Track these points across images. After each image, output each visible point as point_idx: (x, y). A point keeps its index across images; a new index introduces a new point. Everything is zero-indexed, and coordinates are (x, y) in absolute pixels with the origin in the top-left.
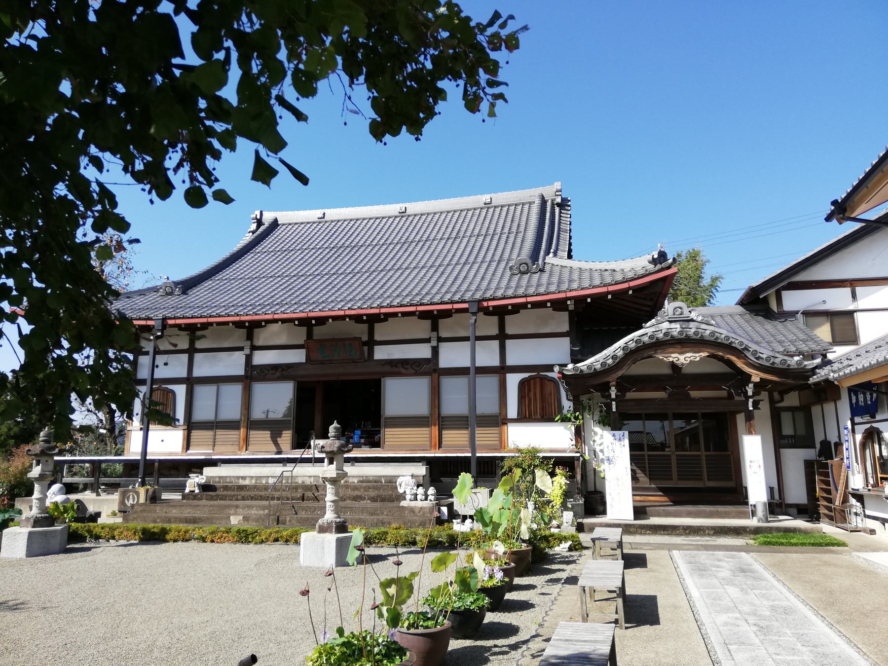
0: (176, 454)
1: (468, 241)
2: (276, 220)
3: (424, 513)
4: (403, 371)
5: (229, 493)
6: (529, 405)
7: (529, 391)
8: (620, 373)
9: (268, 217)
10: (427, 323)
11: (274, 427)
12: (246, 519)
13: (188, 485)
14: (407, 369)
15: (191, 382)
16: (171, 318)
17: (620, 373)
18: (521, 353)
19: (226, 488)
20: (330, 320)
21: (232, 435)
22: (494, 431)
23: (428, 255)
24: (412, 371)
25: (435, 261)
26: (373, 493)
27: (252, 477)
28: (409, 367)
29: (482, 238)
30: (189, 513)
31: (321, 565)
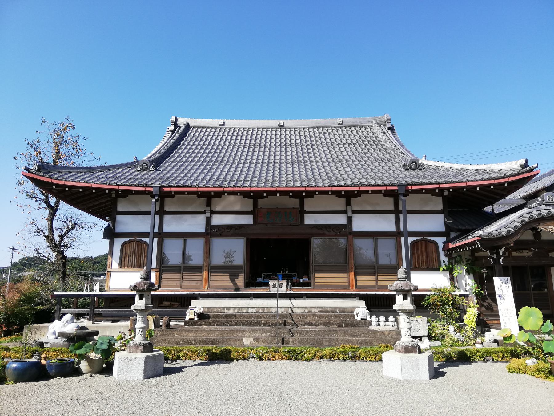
1: (190, 148)
2: (188, 124)
3: (392, 335)
4: (327, 233)
5: (220, 320)
6: (418, 257)
7: (418, 249)
8: (516, 238)
9: (182, 122)
10: (204, 200)
11: (231, 270)
12: (256, 340)
13: (188, 314)
14: (330, 231)
16: (166, 187)
17: (516, 238)
18: (417, 224)
19: (218, 316)
20: (278, 195)
21: (196, 276)
23: (228, 154)
24: (334, 233)
25: (182, 159)
26: (339, 321)
27: (235, 308)
28: (331, 230)
29: (232, 147)
30: (204, 336)
31: (417, 378)
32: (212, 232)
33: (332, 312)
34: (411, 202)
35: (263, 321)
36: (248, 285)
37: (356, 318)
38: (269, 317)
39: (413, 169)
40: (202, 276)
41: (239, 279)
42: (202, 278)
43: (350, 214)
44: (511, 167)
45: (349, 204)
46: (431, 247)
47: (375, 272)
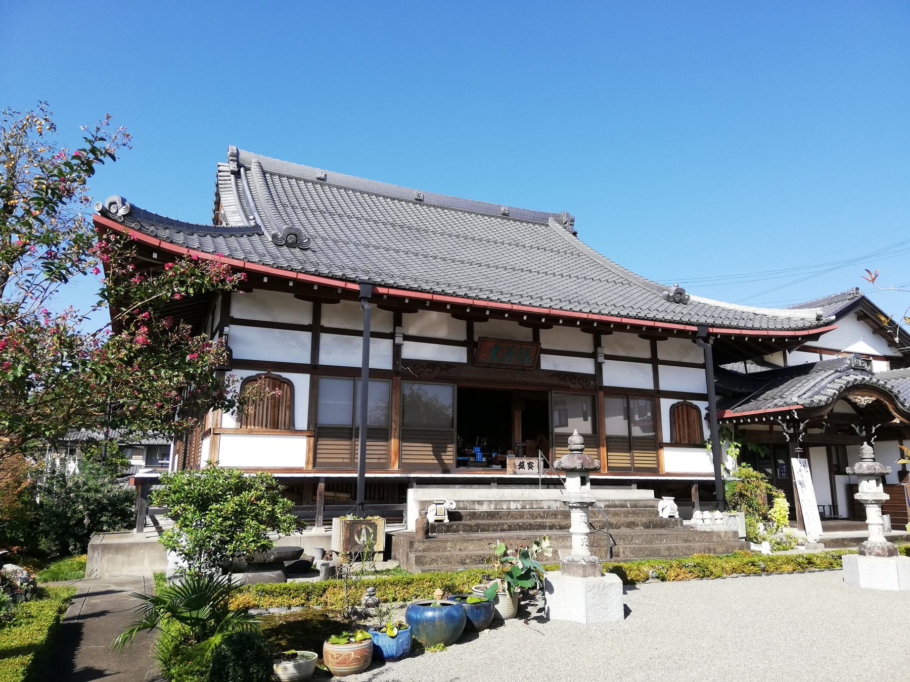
0: (299, 470)
4: (571, 385)
15: (315, 370)
22: (652, 454)
24: (580, 387)
32: (405, 371)
33: (622, 506)
34: (665, 350)
35: (548, 521)
36: (461, 464)
37: (661, 515)
38: (548, 515)
39: (289, 246)
40: (389, 446)
41: (448, 453)
42: (389, 450)
43: (399, 340)
44: (803, 316)
45: (597, 343)
46: (694, 413)
47: (351, 434)
